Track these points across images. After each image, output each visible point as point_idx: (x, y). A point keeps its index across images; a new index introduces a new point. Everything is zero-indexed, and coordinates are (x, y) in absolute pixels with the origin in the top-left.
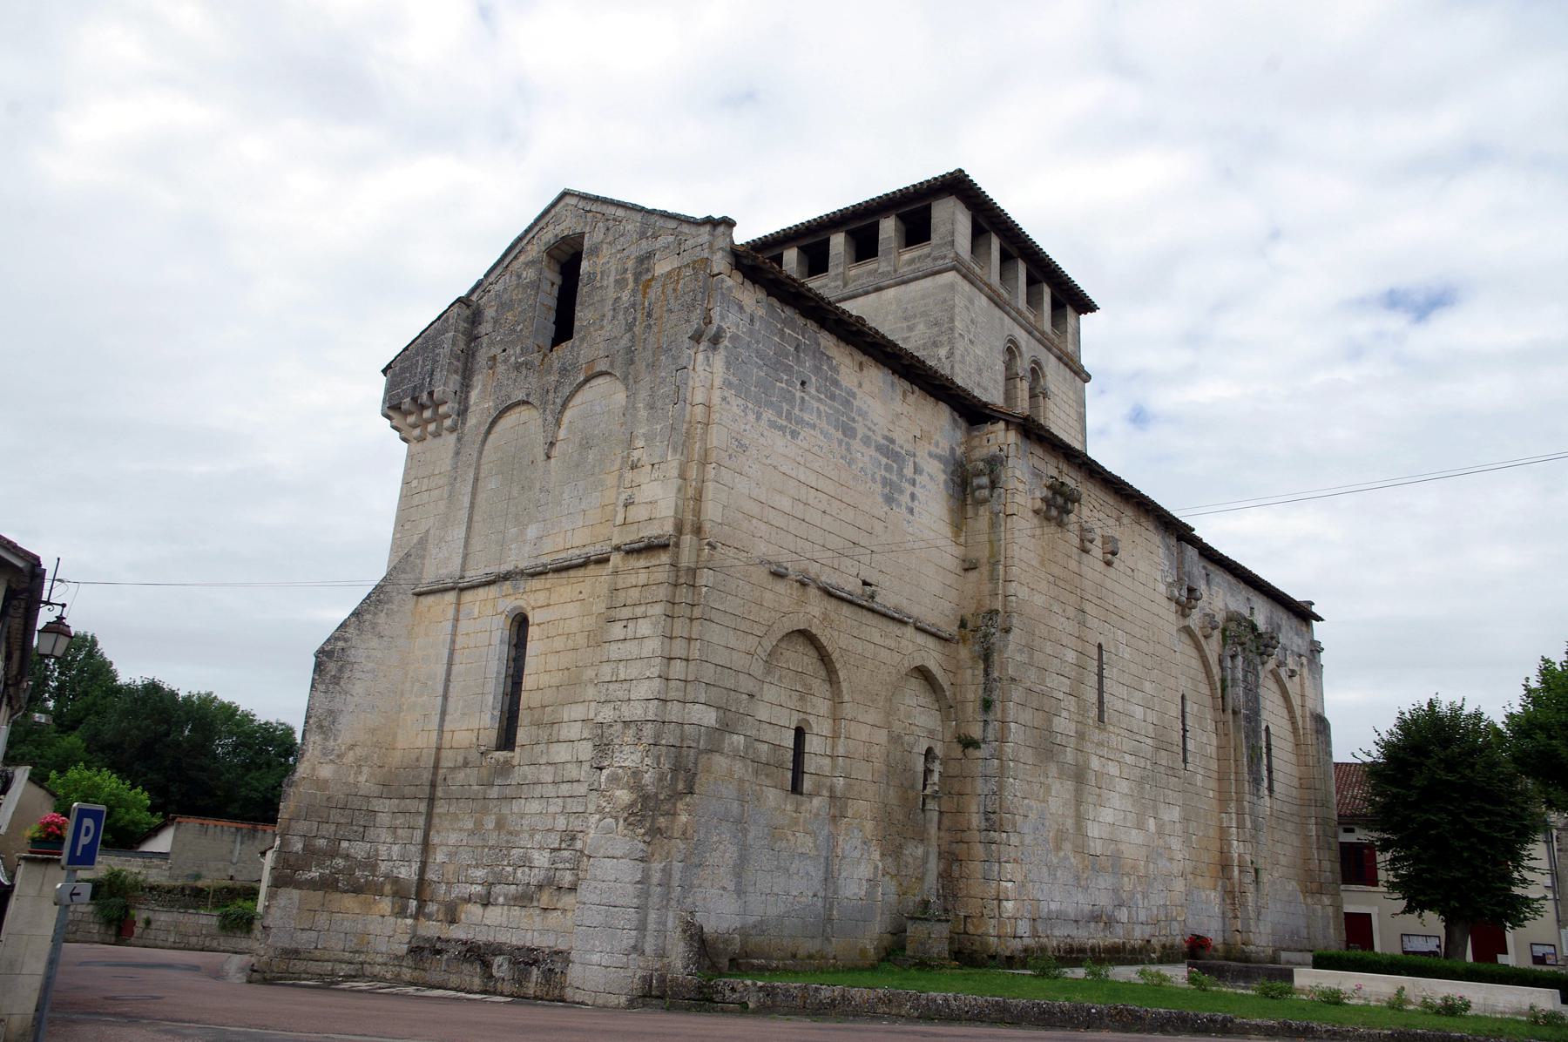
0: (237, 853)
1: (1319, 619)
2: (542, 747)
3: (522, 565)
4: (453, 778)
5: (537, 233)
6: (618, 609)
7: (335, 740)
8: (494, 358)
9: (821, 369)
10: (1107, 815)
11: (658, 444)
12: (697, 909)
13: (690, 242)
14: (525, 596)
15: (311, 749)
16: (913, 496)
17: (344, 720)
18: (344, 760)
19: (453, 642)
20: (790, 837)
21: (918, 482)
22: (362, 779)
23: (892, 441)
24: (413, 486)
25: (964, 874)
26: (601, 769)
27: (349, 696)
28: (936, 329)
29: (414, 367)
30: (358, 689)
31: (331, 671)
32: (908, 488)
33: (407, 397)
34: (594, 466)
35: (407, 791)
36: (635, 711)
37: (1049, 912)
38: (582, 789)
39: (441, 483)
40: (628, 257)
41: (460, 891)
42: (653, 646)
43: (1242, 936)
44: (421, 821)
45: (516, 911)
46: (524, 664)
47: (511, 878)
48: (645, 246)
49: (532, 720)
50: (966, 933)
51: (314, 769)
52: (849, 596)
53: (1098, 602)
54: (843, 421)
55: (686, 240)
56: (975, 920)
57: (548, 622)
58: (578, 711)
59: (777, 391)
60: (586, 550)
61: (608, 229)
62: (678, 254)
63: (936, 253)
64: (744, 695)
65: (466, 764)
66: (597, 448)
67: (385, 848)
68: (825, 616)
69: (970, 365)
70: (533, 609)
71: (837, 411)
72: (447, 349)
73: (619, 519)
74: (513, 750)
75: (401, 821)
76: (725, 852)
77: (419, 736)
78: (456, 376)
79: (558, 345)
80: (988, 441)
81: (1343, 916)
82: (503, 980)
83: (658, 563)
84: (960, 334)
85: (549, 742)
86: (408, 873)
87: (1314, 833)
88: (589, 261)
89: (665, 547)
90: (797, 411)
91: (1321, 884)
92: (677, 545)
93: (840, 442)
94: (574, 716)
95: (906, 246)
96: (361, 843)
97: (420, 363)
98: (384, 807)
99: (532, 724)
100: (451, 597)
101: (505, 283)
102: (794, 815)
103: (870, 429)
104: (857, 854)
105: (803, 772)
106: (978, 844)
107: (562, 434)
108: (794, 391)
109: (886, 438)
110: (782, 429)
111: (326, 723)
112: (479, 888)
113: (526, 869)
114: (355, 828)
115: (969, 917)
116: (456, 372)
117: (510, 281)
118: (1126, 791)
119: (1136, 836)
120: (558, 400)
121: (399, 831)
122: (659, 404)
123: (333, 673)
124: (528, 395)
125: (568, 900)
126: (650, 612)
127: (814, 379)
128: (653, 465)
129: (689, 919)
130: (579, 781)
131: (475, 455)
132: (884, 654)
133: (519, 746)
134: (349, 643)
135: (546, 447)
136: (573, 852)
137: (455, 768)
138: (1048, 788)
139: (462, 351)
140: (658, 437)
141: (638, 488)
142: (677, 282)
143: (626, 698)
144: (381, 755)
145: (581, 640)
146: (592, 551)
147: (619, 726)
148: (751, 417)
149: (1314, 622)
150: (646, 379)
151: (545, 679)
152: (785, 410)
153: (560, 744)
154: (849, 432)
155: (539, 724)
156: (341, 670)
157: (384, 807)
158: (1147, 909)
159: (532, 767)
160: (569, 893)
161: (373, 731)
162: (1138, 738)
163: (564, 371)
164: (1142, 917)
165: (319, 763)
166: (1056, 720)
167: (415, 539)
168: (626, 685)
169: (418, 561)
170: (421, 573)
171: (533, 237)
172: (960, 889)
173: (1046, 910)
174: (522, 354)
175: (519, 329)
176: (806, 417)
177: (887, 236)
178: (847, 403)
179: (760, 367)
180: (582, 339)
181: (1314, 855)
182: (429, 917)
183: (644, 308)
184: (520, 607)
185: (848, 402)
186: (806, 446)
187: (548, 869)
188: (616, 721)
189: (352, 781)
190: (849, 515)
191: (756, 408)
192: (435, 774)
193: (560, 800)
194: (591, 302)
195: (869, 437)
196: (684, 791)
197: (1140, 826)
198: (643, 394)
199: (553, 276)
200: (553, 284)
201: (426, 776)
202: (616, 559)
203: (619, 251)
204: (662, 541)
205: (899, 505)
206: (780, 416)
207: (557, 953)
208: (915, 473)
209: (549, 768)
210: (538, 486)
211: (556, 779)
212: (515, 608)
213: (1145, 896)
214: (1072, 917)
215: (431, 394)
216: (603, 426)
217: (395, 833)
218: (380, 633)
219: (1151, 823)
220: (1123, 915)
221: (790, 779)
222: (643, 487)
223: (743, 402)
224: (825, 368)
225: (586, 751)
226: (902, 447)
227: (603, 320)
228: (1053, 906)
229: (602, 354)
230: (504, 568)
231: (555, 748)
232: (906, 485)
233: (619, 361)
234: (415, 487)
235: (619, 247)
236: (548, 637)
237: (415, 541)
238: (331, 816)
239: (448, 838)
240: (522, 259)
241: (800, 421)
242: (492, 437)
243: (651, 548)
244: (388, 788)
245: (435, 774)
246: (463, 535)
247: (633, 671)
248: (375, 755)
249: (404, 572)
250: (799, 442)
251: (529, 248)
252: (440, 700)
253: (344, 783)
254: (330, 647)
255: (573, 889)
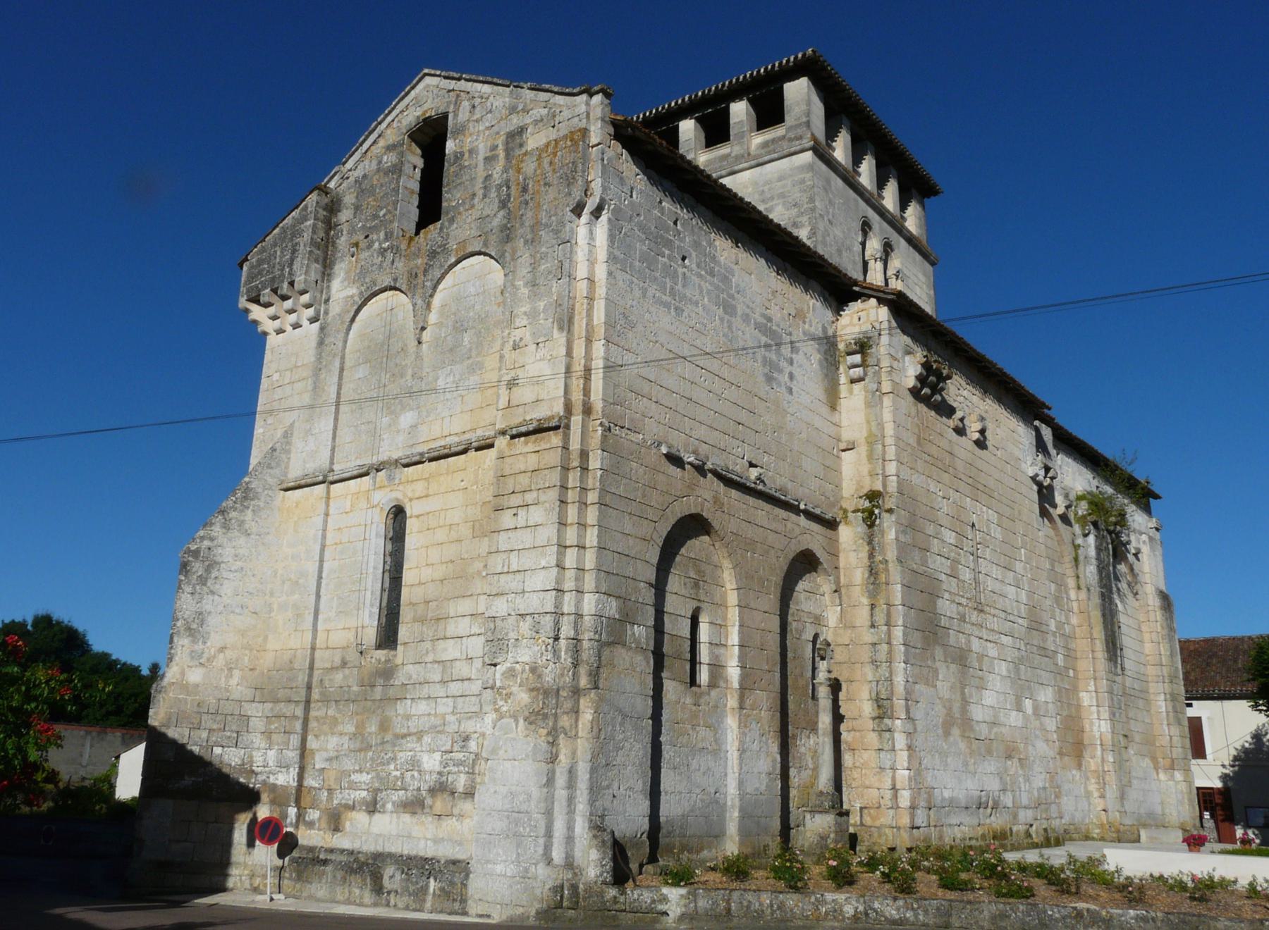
0: (86, 756)
1: (1157, 497)
2: (428, 645)
3: (395, 456)
4: (330, 680)
5: (397, 116)
6: (506, 497)
7: (205, 643)
8: (356, 245)
9: (700, 244)
10: (989, 698)
11: (541, 322)
12: (606, 813)
13: (566, 114)
14: (401, 487)
15: (179, 652)
16: (791, 376)
17: (212, 621)
18: (214, 663)
19: (324, 537)
20: (690, 732)
21: (795, 362)
22: (234, 681)
23: (770, 320)
24: (274, 379)
25: (858, 764)
26: (495, 665)
27: (216, 597)
28: (796, 210)
29: (273, 258)
30: (227, 589)
31: (197, 571)
32: (788, 369)
33: (266, 288)
34: (470, 350)
35: (281, 694)
36: (533, 602)
37: (943, 799)
38: (475, 687)
39: (305, 375)
40: (498, 133)
41: (343, 798)
42: (548, 533)
43: (1107, 816)
44: (298, 726)
45: (407, 818)
46: (403, 558)
47: (399, 783)
48: (516, 121)
49: (414, 616)
50: (862, 824)
51: (183, 673)
52: (738, 479)
53: (970, 481)
54: (723, 298)
55: (560, 112)
56: (872, 811)
57: (428, 513)
58: (465, 606)
59: (660, 266)
60: (467, 436)
61: (474, 107)
62: (553, 127)
63: (791, 135)
64: (642, 584)
65: (344, 664)
66: (474, 330)
67: (260, 754)
68: (716, 500)
69: (831, 245)
70: (411, 500)
71: (717, 288)
72: (307, 236)
73: (503, 403)
74: (395, 649)
75: (276, 725)
76: (630, 750)
77: (293, 636)
78: (316, 265)
79: (425, 226)
80: (859, 319)
81: (1195, 792)
82: (396, 892)
83: (548, 446)
84: (820, 215)
85: (435, 640)
86: (287, 779)
87: (1164, 709)
88: (455, 140)
89: (557, 428)
90: (679, 287)
91: (1173, 760)
92: (568, 427)
93: (722, 319)
94: (461, 610)
95: (758, 130)
96: (234, 749)
97: (278, 253)
98: (254, 710)
99: (415, 620)
100: (321, 488)
101: (364, 168)
102: (694, 708)
103: (748, 307)
104: (755, 746)
105: (700, 663)
106: (872, 732)
107: (433, 318)
108: (676, 266)
109: (763, 315)
110: (667, 305)
111: (194, 626)
112: (364, 794)
113: (416, 774)
114: (229, 734)
115: (866, 808)
116: (317, 261)
117: (370, 166)
118: (1004, 673)
119: (1014, 719)
120: (428, 284)
121: (274, 736)
122: (541, 281)
123: (200, 573)
124: (395, 280)
125: (466, 806)
126: (542, 498)
127: (694, 254)
128: (538, 344)
129: (599, 823)
130: (469, 679)
131: (340, 344)
132: (771, 537)
133: (401, 644)
134: (215, 542)
135: (418, 331)
136: (467, 754)
137: (332, 668)
138: (936, 671)
139: (322, 240)
140: (542, 315)
141: (522, 369)
142: (555, 154)
143: (520, 589)
144: (252, 657)
145: (465, 531)
146: (474, 437)
147: (512, 620)
148: (638, 293)
149: (1151, 500)
150: (525, 259)
151: (427, 573)
152: (668, 286)
153: (447, 641)
154: (729, 309)
155: (421, 620)
156: (208, 570)
157: (256, 711)
158: (1029, 792)
159: (417, 666)
160: (465, 798)
161: (243, 633)
162: (1011, 618)
163: (433, 254)
164: (1025, 801)
165: (188, 666)
166: (940, 602)
167: (279, 433)
168: (519, 577)
169: (284, 456)
170: (287, 467)
171: (393, 121)
172: (854, 779)
173: (940, 798)
174: (386, 239)
175: (382, 213)
176: (688, 293)
177: (739, 120)
178: (726, 279)
179: (643, 242)
180: (452, 221)
181: (1164, 731)
182: (310, 825)
183: (518, 184)
184: (397, 499)
185: (727, 278)
186: (692, 323)
187: (440, 773)
188: (509, 615)
189: (223, 685)
190: (731, 394)
191: (642, 284)
192: (311, 676)
193: (450, 699)
194: (459, 181)
195: (747, 315)
196: (588, 686)
197: (1019, 708)
198: (523, 270)
199: (415, 159)
200: (415, 167)
201: (302, 678)
202: (501, 442)
203: (488, 128)
204: (553, 424)
205: (779, 385)
206: (664, 291)
207: (454, 862)
208: (792, 352)
209: (436, 666)
210: (410, 372)
211: (445, 676)
212: (391, 500)
213: (1027, 780)
214: (963, 804)
215: (292, 284)
216: (478, 307)
217: (270, 738)
218: (246, 531)
219: (1028, 704)
220: (1007, 800)
221: (689, 671)
222: (527, 367)
223: (629, 277)
224: (704, 243)
225: (476, 646)
226: (778, 326)
227: (473, 199)
228: (947, 794)
229: (475, 233)
230: (375, 460)
231: (441, 644)
232: (783, 364)
233: (493, 239)
234: (277, 381)
235: (487, 124)
236: (428, 529)
237: (279, 436)
238: (203, 722)
239: (325, 745)
240: (382, 143)
241: (683, 298)
242: (355, 326)
243: (540, 430)
244: (264, 693)
245: (311, 676)
246: (331, 426)
247: (527, 561)
248: (246, 658)
249: (269, 467)
250: (683, 318)
251: (389, 132)
252: (313, 597)
253: (216, 687)
254: (196, 547)
255: (469, 794)
